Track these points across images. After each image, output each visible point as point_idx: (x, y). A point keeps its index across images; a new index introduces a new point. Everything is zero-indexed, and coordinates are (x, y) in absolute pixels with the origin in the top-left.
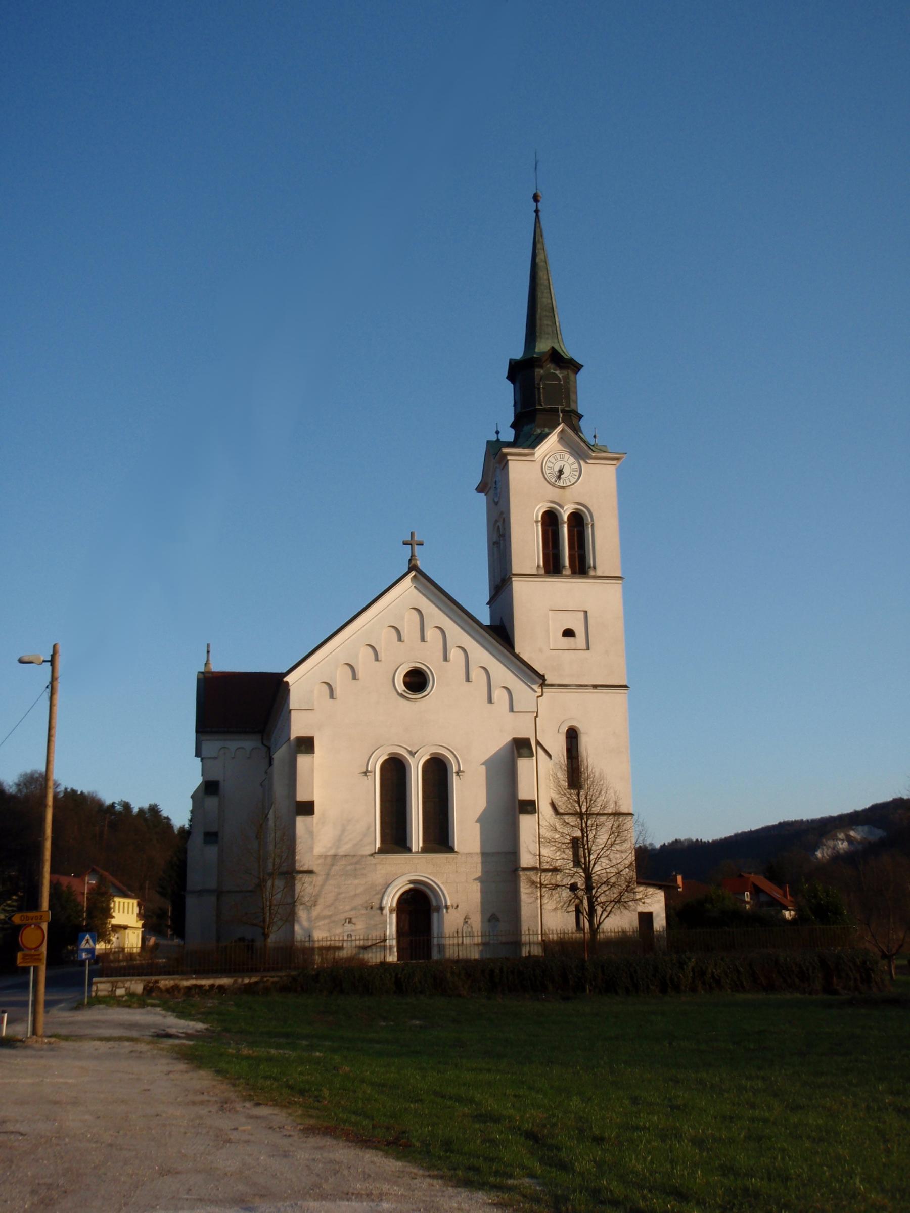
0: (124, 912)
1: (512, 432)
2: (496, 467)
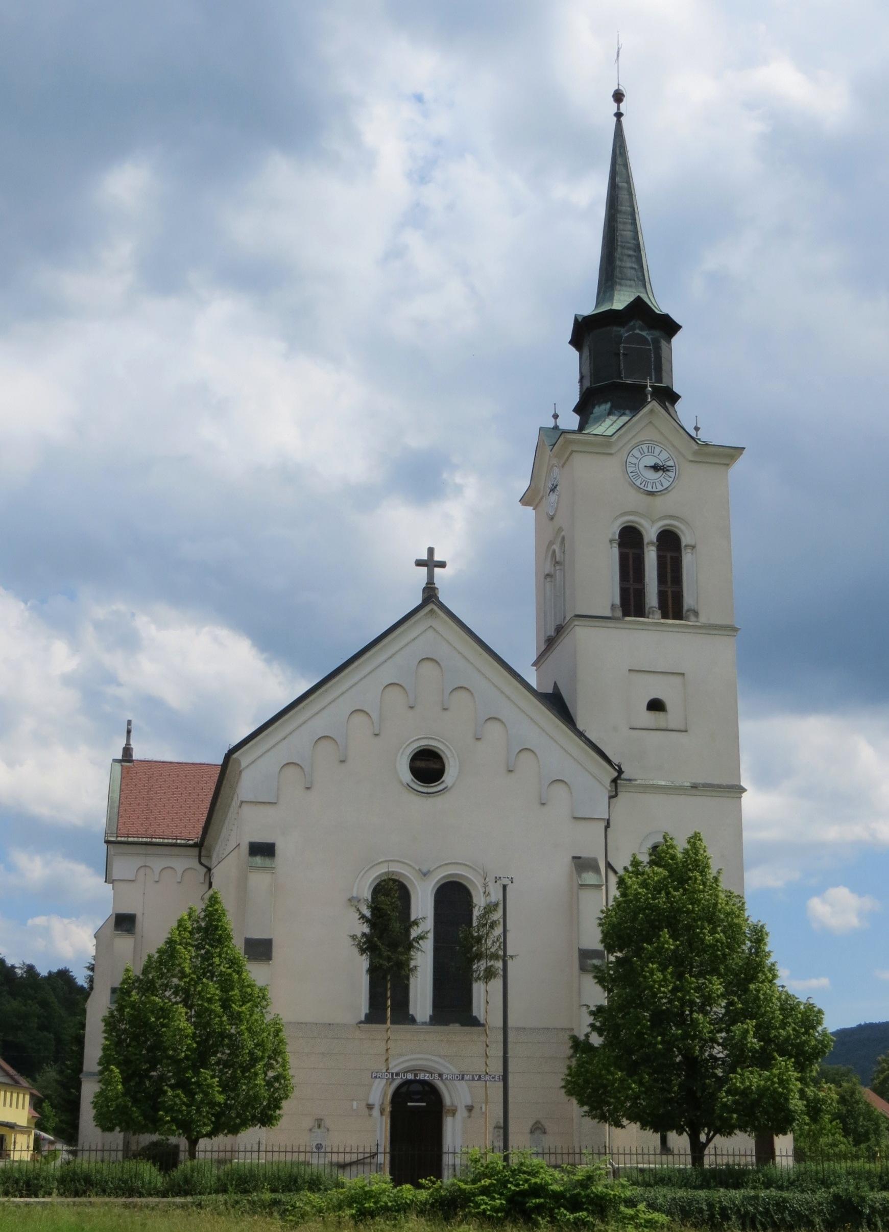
0: (11, 1106)
1: (576, 418)
2: (553, 466)
